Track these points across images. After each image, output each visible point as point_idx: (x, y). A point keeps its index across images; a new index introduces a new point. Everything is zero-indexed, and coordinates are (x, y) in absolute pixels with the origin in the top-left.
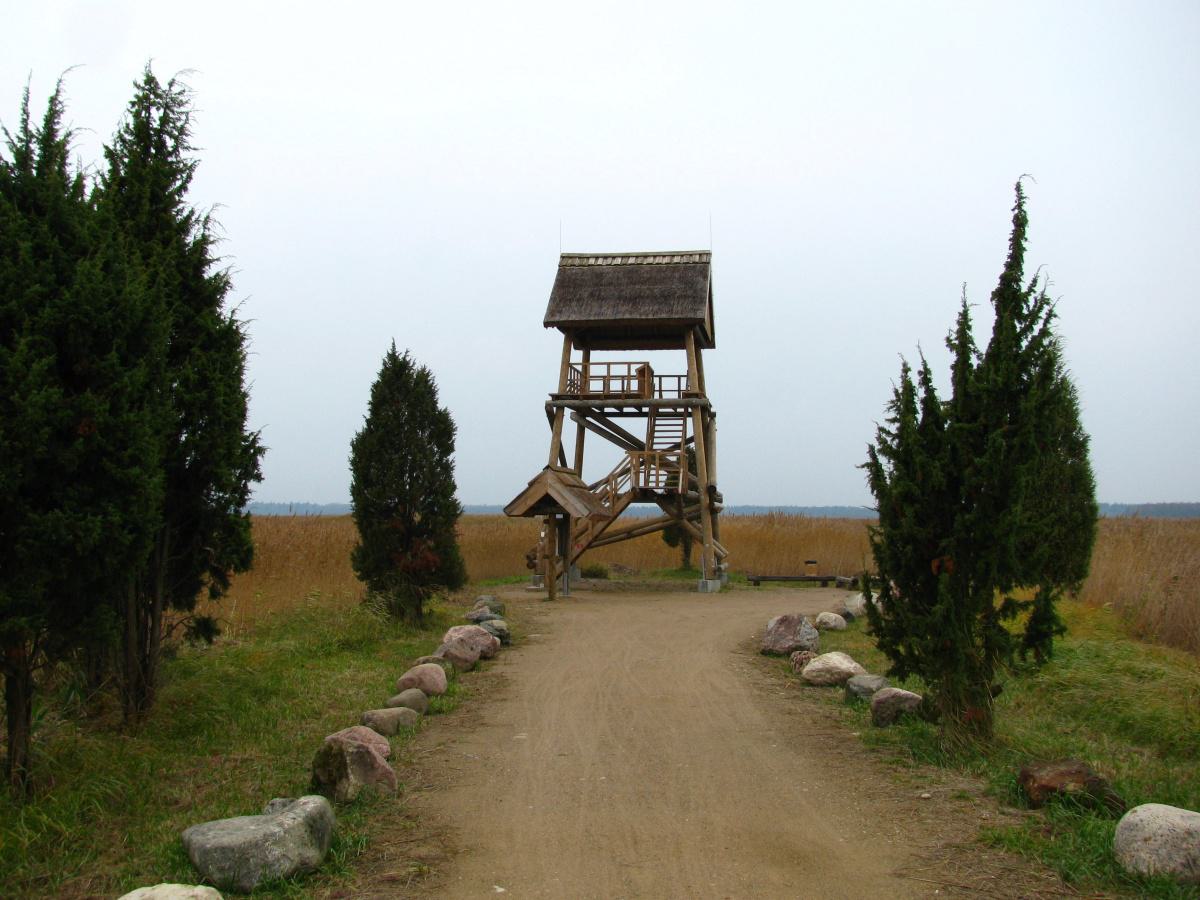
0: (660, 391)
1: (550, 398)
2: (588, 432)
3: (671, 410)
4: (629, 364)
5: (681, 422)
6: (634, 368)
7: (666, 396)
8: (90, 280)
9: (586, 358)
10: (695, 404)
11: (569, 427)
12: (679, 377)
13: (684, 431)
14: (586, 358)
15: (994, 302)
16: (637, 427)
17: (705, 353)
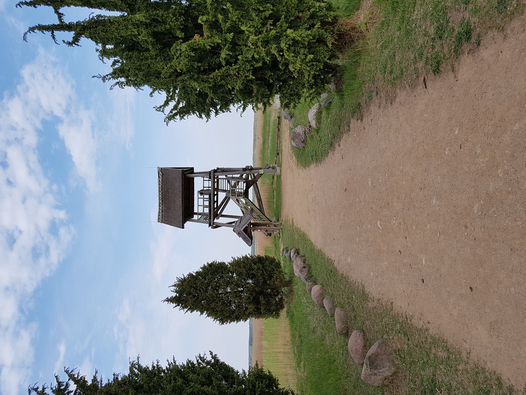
0: (209, 187)
1: (210, 227)
3: (216, 184)
4: (198, 198)
5: (220, 180)
6: (200, 196)
9: (196, 214)
12: (204, 180)
13: (223, 179)
14: (196, 214)
16: (222, 196)
17: (195, 171)
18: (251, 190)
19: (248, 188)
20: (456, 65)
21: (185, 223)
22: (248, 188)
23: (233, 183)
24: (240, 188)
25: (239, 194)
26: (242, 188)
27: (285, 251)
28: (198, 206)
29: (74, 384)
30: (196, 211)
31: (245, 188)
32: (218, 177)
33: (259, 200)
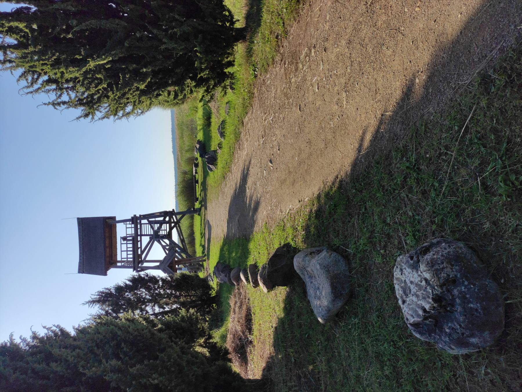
0: (132, 234)
1: (135, 271)
2: (147, 259)
3: (139, 230)
4: (121, 244)
5: (143, 225)
6: (123, 242)
7: (133, 233)
8: (57, 342)
9: (119, 262)
10: (135, 220)
11: (145, 264)
12: (127, 228)
13: (146, 224)
14: (119, 262)
15: (96, 310)
16: (145, 240)
17: (117, 219)
18: (174, 232)
19: (171, 229)
20: (459, 34)
21: (107, 270)
22: (171, 229)
23: (156, 226)
24: (163, 229)
25: (164, 237)
26: (165, 229)
27: (514, 364)
28: (121, 251)
29: (79, 325)
30: (119, 259)
31: (168, 230)
32: (140, 222)
33: (182, 241)
